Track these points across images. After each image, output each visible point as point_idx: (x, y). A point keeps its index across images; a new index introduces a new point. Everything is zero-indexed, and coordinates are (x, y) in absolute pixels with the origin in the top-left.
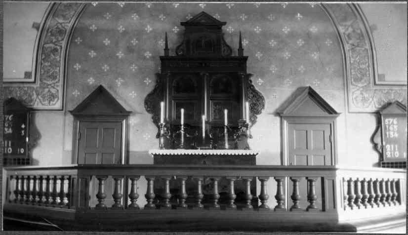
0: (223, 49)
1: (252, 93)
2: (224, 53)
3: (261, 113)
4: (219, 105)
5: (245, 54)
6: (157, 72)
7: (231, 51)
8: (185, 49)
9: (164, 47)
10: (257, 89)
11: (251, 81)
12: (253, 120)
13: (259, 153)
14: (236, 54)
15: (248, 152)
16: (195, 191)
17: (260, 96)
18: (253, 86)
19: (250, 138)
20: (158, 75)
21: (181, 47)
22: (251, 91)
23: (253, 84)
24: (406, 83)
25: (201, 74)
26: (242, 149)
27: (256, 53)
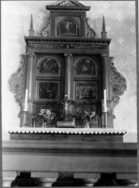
0: (86, 33)
1: (114, 75)
2: (87, 35)
3: (123, 93)
4: (82, 86)
5: (108, 37)
6: (22, 53)
7: (95, 34)
8: (50, 31)
9: (29, 28)
10: (119, 71)
11: (113, 64)
12: (115, 100)
13: (128, 132)
14: (99, 36)
15: (108, 130)
16: (39, 186)
17: (122, 77)
18: (115, 68)
19: (114, 118)
20: (23, 56)
21: (46, 30)
22: (113, 73)
23: (115, 66)
24: (3, 173)
25: (66, 55)
26: (107, 104)
27: (118, 38)
